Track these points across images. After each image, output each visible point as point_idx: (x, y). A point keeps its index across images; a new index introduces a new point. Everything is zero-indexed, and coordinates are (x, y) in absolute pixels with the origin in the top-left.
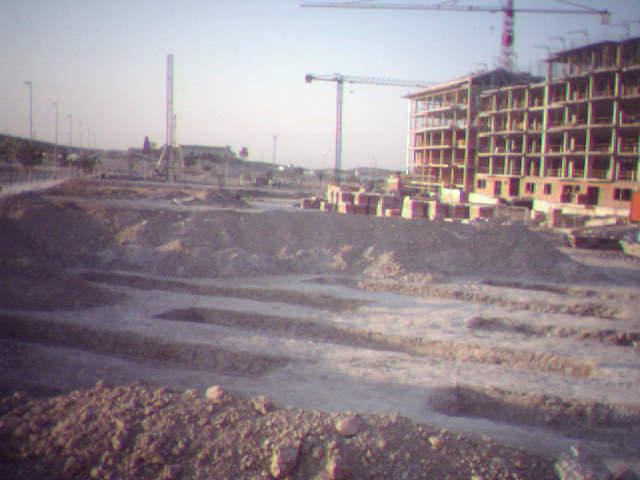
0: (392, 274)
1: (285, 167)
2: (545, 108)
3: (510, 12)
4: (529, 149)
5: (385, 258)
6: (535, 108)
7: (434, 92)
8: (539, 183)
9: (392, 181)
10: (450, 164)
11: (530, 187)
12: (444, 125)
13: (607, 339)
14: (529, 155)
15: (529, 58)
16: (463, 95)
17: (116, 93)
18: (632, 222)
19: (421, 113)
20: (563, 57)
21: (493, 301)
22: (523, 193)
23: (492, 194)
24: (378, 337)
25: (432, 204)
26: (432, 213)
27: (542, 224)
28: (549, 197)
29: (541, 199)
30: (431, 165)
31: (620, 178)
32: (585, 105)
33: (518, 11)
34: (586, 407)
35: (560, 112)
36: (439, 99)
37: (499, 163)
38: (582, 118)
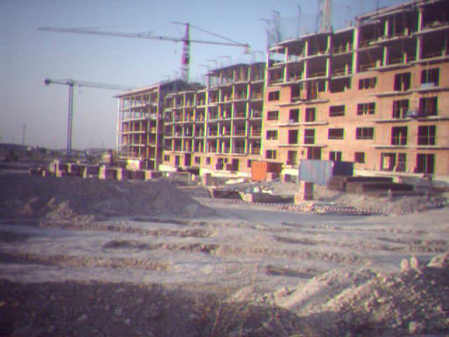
0: (66, 217)
1: (32, 148)
2: (206, 106)
3: (187, 42)
4: (197, 134)
5: (62, 206)
6: (201, 106)
7: (136, 93)
8: (203, 156)
9: (106, 157)
10: (146, 144)
11: (198, 160)
12: (138, 117)
13: (195, 249)
14: (198, 138)
15: (197, 74)
16: (154, 97)
17: (88, 97)
18: (253, 181)
19: (125, 109)
20: (216, 73)
21: (134, 231)
22: (193, 164)
23: (174, 165)
24: (33, 257)
25: (120, 170)
26: (120, 176)
27: (199, 184)
28: (209, 166)
29: (204, 168)
30: (133, 145)
31: (253, 153)
32: (230, 104)
33: (193, 41)
34: (148, 287)
35: (215, 108)
36: (138, 99)
37: (178, 142)
38: (229, 114)
